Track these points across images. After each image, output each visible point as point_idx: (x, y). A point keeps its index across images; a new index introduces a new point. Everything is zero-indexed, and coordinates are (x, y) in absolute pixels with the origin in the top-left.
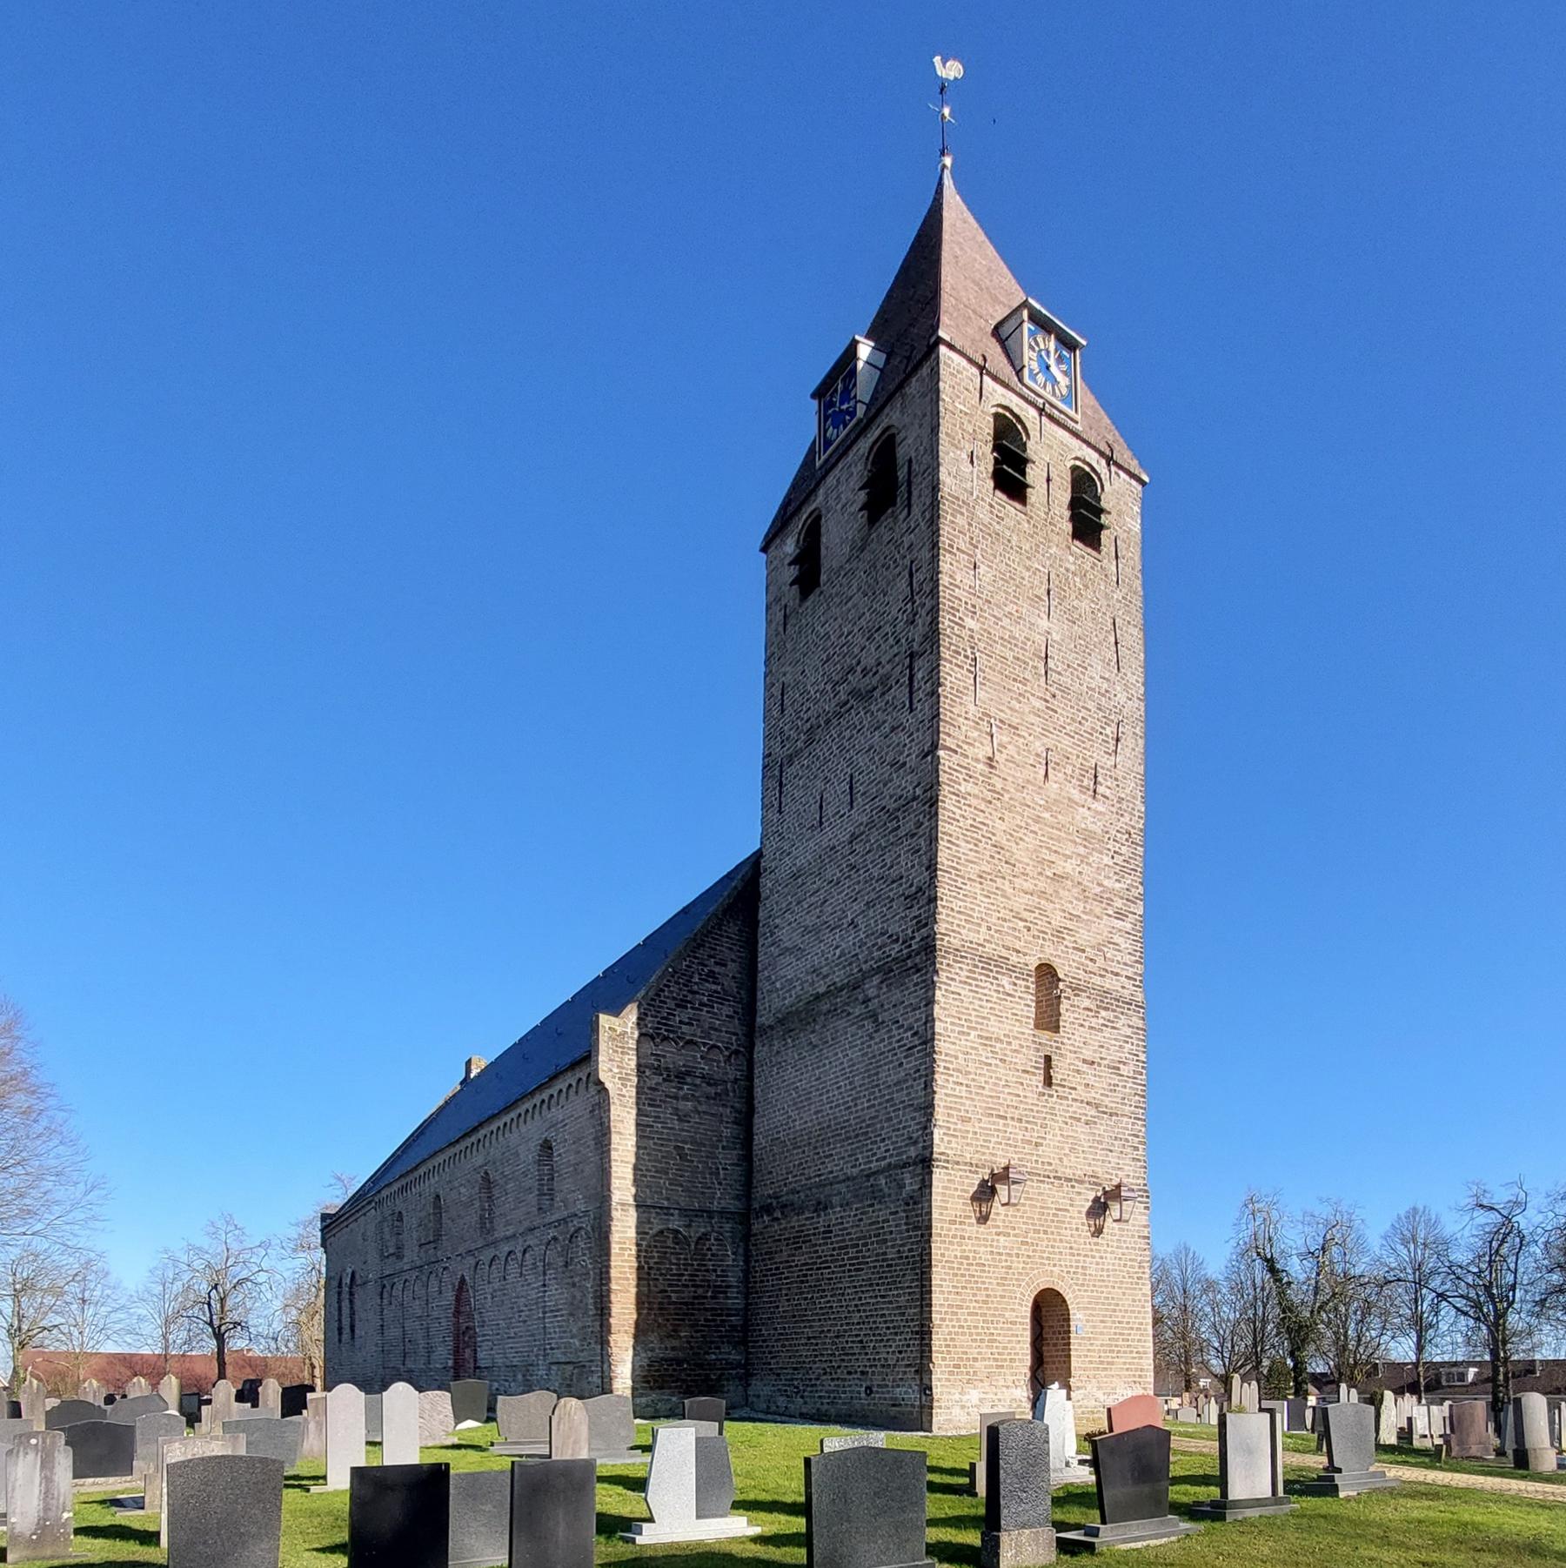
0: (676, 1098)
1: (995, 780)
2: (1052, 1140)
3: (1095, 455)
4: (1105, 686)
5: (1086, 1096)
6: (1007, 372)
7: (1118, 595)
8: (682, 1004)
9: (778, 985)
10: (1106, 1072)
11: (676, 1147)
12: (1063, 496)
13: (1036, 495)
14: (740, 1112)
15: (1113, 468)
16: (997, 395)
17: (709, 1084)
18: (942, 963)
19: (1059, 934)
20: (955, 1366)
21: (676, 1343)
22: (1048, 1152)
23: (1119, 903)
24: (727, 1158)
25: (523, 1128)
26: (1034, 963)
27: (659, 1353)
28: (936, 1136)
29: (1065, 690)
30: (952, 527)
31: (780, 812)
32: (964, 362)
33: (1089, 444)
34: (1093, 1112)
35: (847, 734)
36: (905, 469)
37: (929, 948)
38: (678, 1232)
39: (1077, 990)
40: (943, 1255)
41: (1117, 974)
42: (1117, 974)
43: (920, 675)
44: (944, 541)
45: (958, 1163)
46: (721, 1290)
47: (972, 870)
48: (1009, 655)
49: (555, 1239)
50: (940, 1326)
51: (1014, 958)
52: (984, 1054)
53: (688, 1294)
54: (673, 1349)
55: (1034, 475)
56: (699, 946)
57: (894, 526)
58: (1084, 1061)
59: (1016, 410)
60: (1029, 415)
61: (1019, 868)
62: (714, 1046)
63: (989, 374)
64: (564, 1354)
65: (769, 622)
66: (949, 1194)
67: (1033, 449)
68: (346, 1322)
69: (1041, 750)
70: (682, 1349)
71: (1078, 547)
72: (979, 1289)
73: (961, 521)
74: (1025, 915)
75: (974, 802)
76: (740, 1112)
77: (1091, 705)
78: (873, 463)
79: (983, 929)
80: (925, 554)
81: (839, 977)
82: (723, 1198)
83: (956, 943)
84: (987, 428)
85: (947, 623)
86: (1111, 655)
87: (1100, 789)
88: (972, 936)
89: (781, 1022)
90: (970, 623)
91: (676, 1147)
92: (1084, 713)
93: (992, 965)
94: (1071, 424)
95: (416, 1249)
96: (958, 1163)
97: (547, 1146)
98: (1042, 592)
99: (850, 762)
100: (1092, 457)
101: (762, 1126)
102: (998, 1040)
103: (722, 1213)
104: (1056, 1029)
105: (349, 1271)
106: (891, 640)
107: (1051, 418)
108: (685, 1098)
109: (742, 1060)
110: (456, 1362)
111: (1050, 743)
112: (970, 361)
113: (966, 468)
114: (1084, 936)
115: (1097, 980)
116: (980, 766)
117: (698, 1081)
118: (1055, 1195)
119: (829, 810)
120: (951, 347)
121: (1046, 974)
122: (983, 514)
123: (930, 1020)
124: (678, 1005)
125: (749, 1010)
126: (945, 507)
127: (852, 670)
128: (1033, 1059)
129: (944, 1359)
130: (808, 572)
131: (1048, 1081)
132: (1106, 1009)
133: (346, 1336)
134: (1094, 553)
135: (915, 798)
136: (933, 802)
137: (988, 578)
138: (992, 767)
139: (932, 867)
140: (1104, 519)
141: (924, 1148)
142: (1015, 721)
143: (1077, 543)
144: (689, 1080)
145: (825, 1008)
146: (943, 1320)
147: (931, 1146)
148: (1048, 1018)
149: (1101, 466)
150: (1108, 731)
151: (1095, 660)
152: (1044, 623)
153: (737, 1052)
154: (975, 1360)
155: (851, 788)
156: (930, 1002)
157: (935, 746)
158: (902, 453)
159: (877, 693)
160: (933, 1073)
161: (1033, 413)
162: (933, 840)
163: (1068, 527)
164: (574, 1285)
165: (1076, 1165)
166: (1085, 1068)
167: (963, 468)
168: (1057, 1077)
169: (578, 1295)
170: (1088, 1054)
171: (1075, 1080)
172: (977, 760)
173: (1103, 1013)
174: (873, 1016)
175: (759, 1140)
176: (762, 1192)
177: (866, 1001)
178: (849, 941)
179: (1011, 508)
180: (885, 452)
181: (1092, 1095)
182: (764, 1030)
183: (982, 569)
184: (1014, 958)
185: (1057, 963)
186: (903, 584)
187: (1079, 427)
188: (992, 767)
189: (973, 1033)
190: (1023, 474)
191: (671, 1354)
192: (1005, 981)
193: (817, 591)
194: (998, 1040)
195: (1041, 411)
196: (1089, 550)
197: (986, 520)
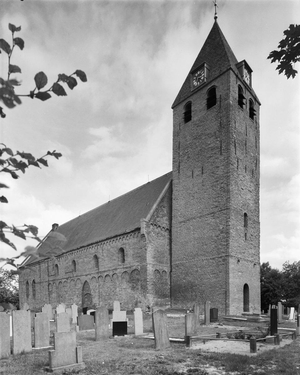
69: (245, 166)
78: (208, 93)
93: (238, 213)
130: (188, 117)
131: (246, 239)
133: (30, 297)
143: (250, 118)
149: (254, 101)
195: (245, 87)
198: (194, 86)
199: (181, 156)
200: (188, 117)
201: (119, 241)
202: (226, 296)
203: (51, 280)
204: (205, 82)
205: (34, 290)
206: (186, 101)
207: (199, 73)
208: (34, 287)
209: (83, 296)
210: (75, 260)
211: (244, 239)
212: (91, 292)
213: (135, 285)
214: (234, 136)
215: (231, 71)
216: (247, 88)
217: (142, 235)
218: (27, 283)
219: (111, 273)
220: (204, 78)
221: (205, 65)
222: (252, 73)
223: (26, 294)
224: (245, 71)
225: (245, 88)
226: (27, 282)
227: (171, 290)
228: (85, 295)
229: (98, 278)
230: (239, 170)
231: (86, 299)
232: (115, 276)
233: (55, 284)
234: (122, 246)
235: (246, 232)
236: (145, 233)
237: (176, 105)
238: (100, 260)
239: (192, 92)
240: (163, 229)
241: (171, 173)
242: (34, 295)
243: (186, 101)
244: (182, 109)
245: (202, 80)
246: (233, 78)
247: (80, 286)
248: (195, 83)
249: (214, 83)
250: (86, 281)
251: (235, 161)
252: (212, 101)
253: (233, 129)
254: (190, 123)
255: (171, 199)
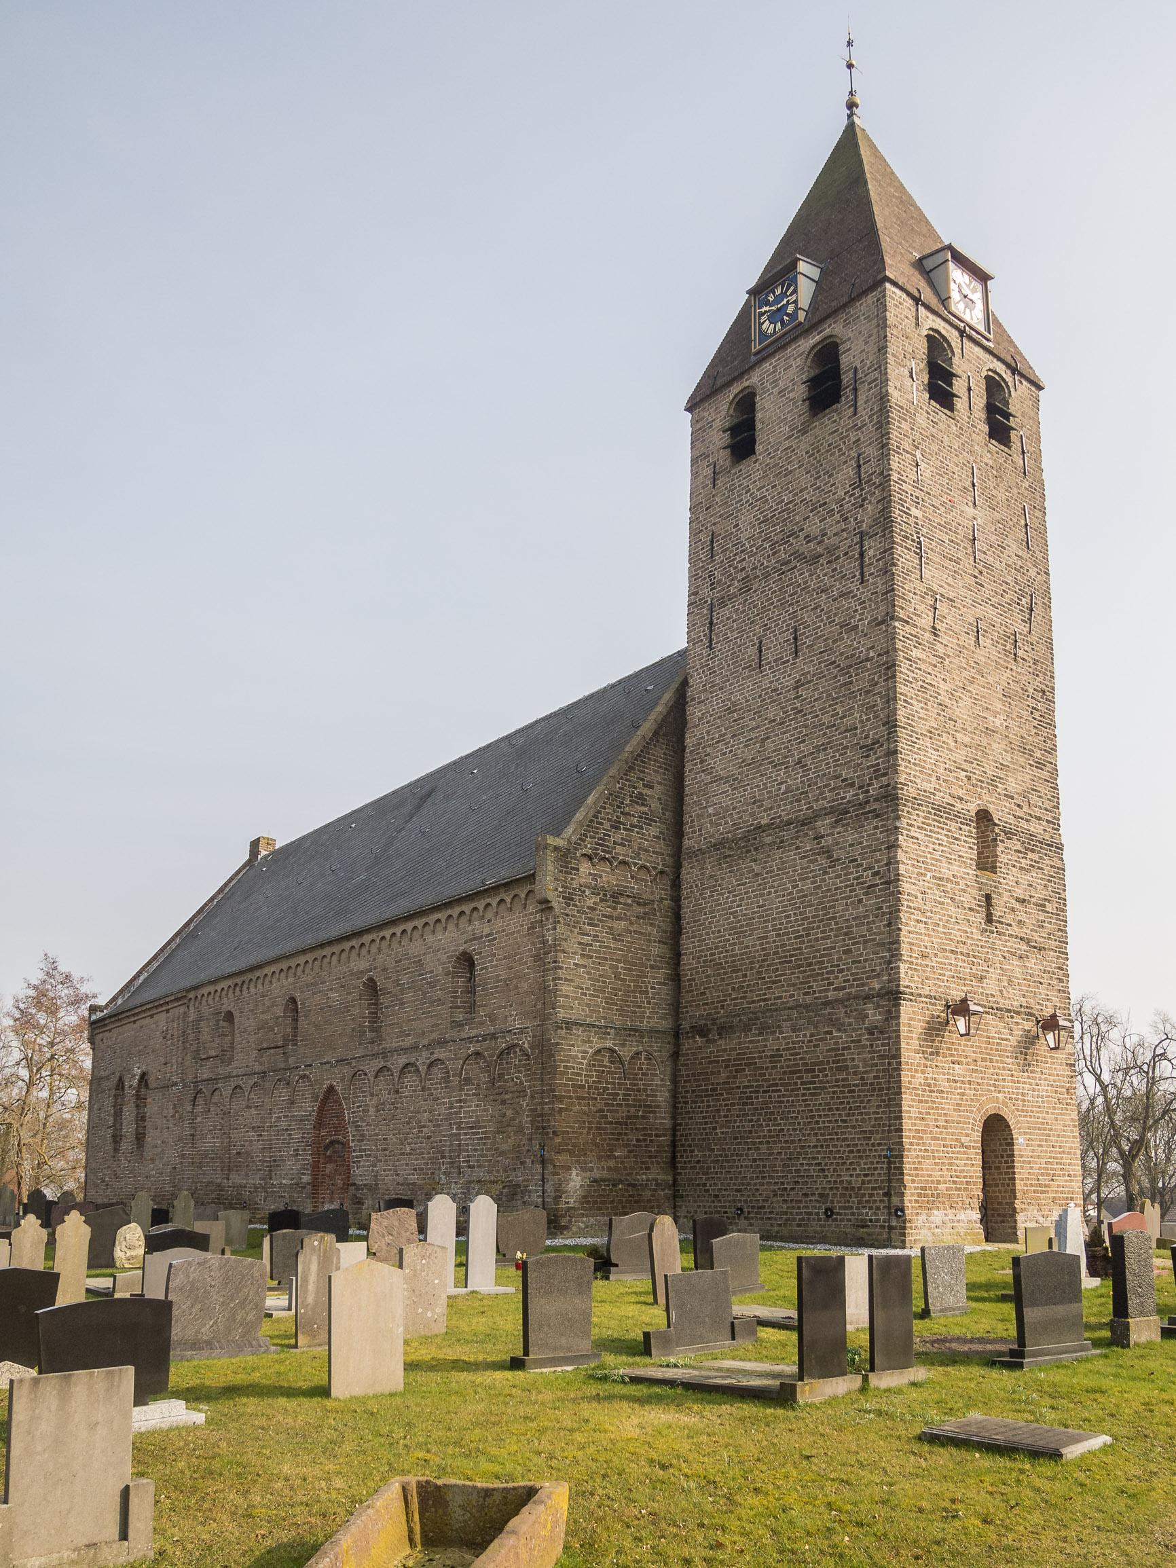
0: (610, 917)
1: (938, 647)
2: (993, 974)
3: (1004, 367)
4: (1019, 563)
5: (1015, 930)
6: (934, 302)
7: (1026, 484)
8: (616, 826)
9: (710, 810)
10: (1033, 909)
11: (612, 966)
12: (980, 401)
13: (960, 404)
14: (666, 932)
15: (1017, 377)
16: (930, 322)
17: (639, 904)
18: (904, 810)
19: (993, 782)
20: (922, 1188)
21: (611, 1163)
22: (991, 986)
23: (1038, 754)
24: (657, 979)
25: (430, 939)
26: (973, 808)
27: (597, 1174)
28: (902, 971)
29: (988, 567)
30: (899, 431)
31: (710, 646)
32: (904, 296)
33: (999, 359)
34: (1025, 947)
35: (790, 590)
36: (851, 374)
37: (891, 797)
38: (614, 1051)
39: (1009, 834)
40: (910, 1082)
41: (1039, 819)
42: (1039, 819)
43: (871, 553)
44: (893, 444)
45: (920, 996)
46: (650, 1109)
47: (922, 727)
48: (946, 538)
49: (477, 1054)
50: (909, 1150)
51: (959, 806)
52: (937, 894)
53: (622, 1113)
54: (609, 1169)
55: (959, 386)
56: (631, 768)
57: (838, 419)
58: (1018, 900)
59: (943, 332)
60: (952, 335)
61: (959, 725)
62: (643, 867)
63: (924, 305)
64: (490, 1172)
65: (695, 474)
66: (912, 1019)
67: (959, 365)
68: (128, 1129)
69: (972, 620)
70: (617, 1170)
71: (994, 446)
72: (940, 1115)
73: (905, 426)
74: (965, 766)
75: (923, 667)
76: (666, 932)
77: (1009, 579)
78: (813, 361)
79: (934, 779)
80: (872, 451)
81: (784, 812)
82: (654, 1017)
83: (913, 792)
84: (922, 347)
85: (897, 512)
86: (1022, 536)
87: (1020, 653)
88: (926, 786)
89: (716, 846)
90: (914, 512)
91: (612, 966)
92: (1004, 587)
93: (941, 811)
94: (984, 342)
95: (255, 1053)
96: (920, 996)
97: (467, 961)
98: (968, 484)
99: (794, 616)
100: (1001, 368)
101: (688, 945)
102: (948, 880)
103: (652, 1032)
104: (993, 869)
105: (138, 1072)
106: (837, 517)
107: (970, 338)
108: (619, 918)
109: (666, 882)
110: (315, 1177)
111: (980, 614)
112: (909, 294)
113: (908, 382)
114: (1013, 786)
115: (1024, 824)
116: (927, 635)
117: (629, 901)
118: (994, 1026)
119: (770, 655)
120: (895, 284)
121: (984, 817)
122: (922, 420)
123: (892, 862)
124: (612, 826)
125: (677, 831)
126: (894, 415)
127: (793, 534)
128: (970, 898)
129: (913, 1181)
130: (742, 441)
131: (989, 919)
132: (1033, 851)
133: (126, 1145)
134: (1006, 449)
135: (868, 660)
136: (891, 666)
137: (928, 474)
138: (936, 635)
139: (891, 724)
140: (1012, 422)
141: (890, 981)
142: (951, 595)
143: (993, 442)
144: (622, 900)
145: (768, 840)
146: (911, 1144)
147: (898, 979)
148: (986, 863)
149: (1008, 376)
150: (1024, 601)
151: (1009, 541)
152: (970, 511)
153: (662, 872)
154: (938, 1182)
155: (795, 638)
156: (893, 846)
157: (891, 616)
158: (845, 360)
159: (823, 560)
160: (899, 911)
161: (956, 333)
162: (891, 698)
163: (986, 429)
164: (503, 1102)
165: (1014, 999)
166: (1017, 906)
167: (906, 385)
168: (997, 913)
169: (509, 1113)
170: (1019, 893)
171: (1009, 918)
172: (924, 630)
173: (1030, 855)
174: (828, 852)
175: (688, 962)
176: (694, 1013)
177: (818, 837)
178: (796, 780)
179: (942, 415)
180: (828, 355)
181: (1025, 931)
182: (693, 854)
183: (923, 466)
184: (959, 806)
185: (991, 808)
186: (849, 471)
187: (991, 345)
188: (936, 635)
189: (929, 874)
190: (950, 385)
191: (605, 1174)
192: (953, 826)
193: (753, 458)
194: (948, 880)
195: (962, 333)
196: (1002, 447)
197: (924, 425)
198: (763, 335)
199: (718, 582)
200: (742, 441)
201: (457, 925)
202: (889, 1168)
203: (205, 1077)
204: (800, 323)
205: (141, 1118)
206: (736, 389)
207: (778, 291)
208: (140, 1100)
209: (316, 1152)
210: (297, 995)
211: (980, 917)
212: (345, 1136)
213: (509, 1113)
214: (914, 512)
215: (888, 285)
216: (970, 338)
217: (540, 902)
218: (120, 1084)
219: (422, 1060)
220: (797, 309)
221: (803, 267)
222: (989, 283)
223: (110, 1131)
224: (957, 276)
225: (962, 336)
226: (121, 1079)
227: (674, 1135)
228: (326, 1148)
229: (376, 1077)
230: (944, 638)
231: (329, 1168)
232: (437, 1073)
233: (216, 1093)
234: (473, 947)
235: (987, 890)
236: (551, 895)
237: (702, 401)
238: (385, 1001)
239: (756, 354)
240: (643, 875)
241: (682, 654)
242: (140, 1138)
243: (736, 389)
244: (721, 412)
245: (788, 315)
246: (897, 305)
247: (307, 1107)
248: (768, 327)
249: (834, 328)
250: (331, 1089)
251: (921, 607)
252: (826, 387)
253: (905, 487)
254: (753, 469)
255: (679, 749)
